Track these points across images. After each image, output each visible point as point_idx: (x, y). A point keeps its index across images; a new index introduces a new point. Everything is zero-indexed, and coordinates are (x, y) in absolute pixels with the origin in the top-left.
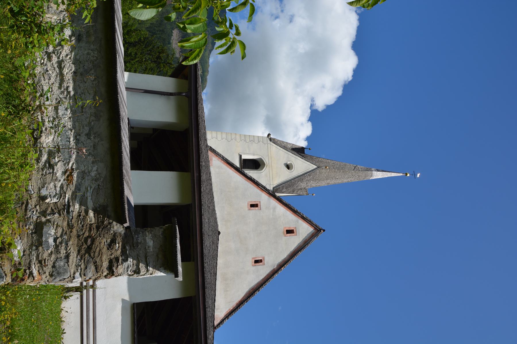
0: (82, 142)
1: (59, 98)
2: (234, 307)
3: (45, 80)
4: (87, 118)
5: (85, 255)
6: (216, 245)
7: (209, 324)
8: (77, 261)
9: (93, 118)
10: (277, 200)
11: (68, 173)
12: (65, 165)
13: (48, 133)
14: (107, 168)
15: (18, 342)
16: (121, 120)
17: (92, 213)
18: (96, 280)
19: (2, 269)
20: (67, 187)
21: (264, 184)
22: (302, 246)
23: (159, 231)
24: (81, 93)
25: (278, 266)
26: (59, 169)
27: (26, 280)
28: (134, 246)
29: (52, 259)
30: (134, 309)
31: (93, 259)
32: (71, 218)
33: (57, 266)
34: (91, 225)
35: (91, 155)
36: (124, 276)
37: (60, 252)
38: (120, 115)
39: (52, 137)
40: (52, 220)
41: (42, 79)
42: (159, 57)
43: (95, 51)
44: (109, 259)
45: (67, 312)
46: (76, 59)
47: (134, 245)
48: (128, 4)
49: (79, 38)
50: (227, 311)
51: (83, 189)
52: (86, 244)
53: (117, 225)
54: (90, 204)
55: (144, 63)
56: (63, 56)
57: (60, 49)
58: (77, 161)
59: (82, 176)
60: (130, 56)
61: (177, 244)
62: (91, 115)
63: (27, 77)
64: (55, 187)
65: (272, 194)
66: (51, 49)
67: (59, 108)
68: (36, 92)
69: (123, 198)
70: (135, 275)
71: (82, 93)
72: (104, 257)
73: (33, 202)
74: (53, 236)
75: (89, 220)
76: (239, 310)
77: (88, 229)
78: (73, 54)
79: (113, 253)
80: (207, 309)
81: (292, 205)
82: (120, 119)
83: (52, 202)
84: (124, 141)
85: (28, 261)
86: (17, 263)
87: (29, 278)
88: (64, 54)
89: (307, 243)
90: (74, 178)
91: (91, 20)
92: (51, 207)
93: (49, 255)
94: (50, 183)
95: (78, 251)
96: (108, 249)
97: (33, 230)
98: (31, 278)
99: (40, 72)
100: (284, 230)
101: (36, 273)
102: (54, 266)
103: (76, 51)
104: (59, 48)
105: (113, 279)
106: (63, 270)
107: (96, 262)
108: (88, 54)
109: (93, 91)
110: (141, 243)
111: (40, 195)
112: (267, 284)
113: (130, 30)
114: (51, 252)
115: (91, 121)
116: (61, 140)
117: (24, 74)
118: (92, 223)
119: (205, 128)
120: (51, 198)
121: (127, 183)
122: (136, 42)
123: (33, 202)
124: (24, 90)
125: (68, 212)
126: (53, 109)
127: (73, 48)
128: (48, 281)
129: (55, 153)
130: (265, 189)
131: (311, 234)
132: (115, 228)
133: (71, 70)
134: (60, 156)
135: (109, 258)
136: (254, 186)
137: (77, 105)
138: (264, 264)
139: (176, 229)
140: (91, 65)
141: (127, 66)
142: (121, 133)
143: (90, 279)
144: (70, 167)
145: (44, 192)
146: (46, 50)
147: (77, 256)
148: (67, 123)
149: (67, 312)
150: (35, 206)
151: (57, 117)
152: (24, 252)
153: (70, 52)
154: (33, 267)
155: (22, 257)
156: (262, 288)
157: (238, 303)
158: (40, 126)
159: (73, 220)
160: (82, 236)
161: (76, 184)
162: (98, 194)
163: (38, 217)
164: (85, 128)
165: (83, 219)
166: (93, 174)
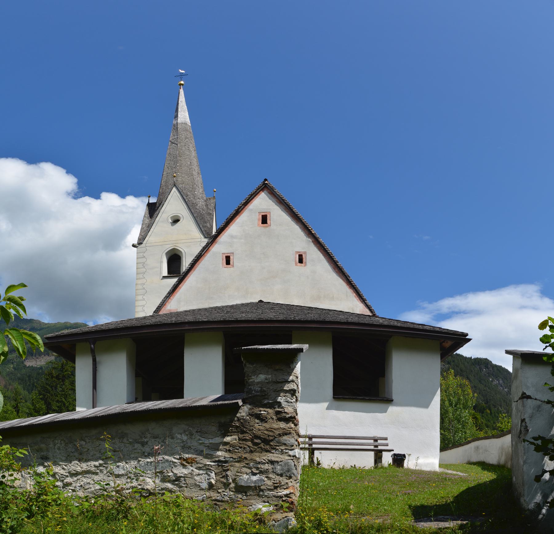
0: (151, 450)
1: (107, 474)
2: (354, 291)
3: (91, 488)
4: (125, 446)
5: (272, 445)
6: (275, 305)
7: (367, 320)
8: (277, 453)
9: (125, 440)
10: (221, 233)
11: (184, 463)
12: (176, 466)
13: (144, 483)
14: (178, 424)
15: (352, 505)
16: (124, 411)
17: (227, 438)
18: (300, 434)
19: (281, 520)
20: (199, 463)
21: (200, 248)
22: (286, 207)
23: (249, 368)
24: (100, 454)
25: (309, 237)
26: (180, 471)
27: (292, 500)
28: (264, 395)
29: (274, 477)
30: (339, 398)
31: (275, 437)
32: (231, 459)
33: (281, 472)
34: (239, 439)
35: (165, 440)
36: (297, 406)
37: (267, 469)
38: (119, 413)
39: (148, 479)
40: (234, 477)
41: (89, 490)
42: (57, 377)
43: (55, 443)
44: (277, 421)
45: (335, 463)
46: (65, 460)
47: (264, 394)
48: (7, 415)
49: (45, 459)
50: (357, 299)
51: (201, 448)
52: (259, 444)
53: (240, 413)
54: (217, 440)
55: (67, 392)
56: (64, 472)
57: (59, 476)
58: (171, 455)
59: (187, 449)
60: (61, 407)
61: (264, 348)
62: (122, 442)
63: (89, 504)
64: (199, 475)
65: (213, 239)
66: (59, 484)
67: (117, 474)
68: (103, 495)
69: (211, 406)
70: (297, 394)
71: (100, 452)
72: (274, 426)
73: (214, 495)
74: (250, 476)
75: (235, 441)
76: (357, 287)
77: (244, 442)
78: (61, 463)
79: (271, 417)
80: (349, 321)
81: (227, 215)
82: (124, 412)
83: (214, 477)
84: (148, 407)
85: (274, 498)
86: (275, 508)
87: (291, 498)
88: (62, 472)
89: (282, 201)
90: (189, 457)
91: (24, 449)
92: (220, 478)
93: (269, 479)
94: (195, 479)
95: (267, 452)
96: (266, 422)
97: (243, 495)
98: (291, 496)
99: (83, 492)
100: (261, 227)
101: (286, 491)
102: (281, 475)
103: (58, 460)
104: (57, 476)
105: (299, 417)
106: (286, 467)
107: (279, 434)
108: (59, 449)
109: (97, 442)
110: (261, 388)
111: (208, 489)
112: (330, 251)
113: (33, 409)
114: (267, 477)
115: (128, 442)
116: (150, 470)
117: (87, 507)
118: (238, 438)
119: (130, 320)
120: (210, 479)
121: (194, 402)
122: (45, 403)
123: (214, 495)
124: (103, 505)
125: (226, 462)
126: (119, 479)
127: (56, 464)
128: (295, 480)
129: (164, 476)
130: (206, 248)
131: (269, 195)
132: (243, 414)
133: (78, 464)
134: (167, 471)
135: (276, 422)
136: (202, 261)
137: (112, 456)
138: (305, 253)
139: (247, 348)
140: (70, 445)
141: (72, 409)
142: (139, 411)
143: (297, 440)
144: (178, 461)
145: (205, 485)
146: (61, 488)
147: (272, 453)
148: (132, 465)
149: (335, 463)
150: (219, 493)
151: (127, 475)
152: (265, 502)
153: (60, 466)
154: (280, 494)
155: (270, 504)
156: (335, 257)
157: (349, 287)
158: (137, 490)
159: (234, 457)
160: (251, 449)
161: (196, 455)
162: (206, 432)
163: (230, 490)
164: (136, 447)
165: (233, 447)
166: (185, 438)
